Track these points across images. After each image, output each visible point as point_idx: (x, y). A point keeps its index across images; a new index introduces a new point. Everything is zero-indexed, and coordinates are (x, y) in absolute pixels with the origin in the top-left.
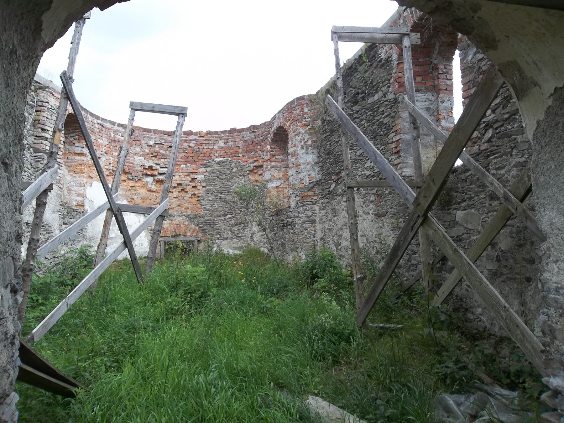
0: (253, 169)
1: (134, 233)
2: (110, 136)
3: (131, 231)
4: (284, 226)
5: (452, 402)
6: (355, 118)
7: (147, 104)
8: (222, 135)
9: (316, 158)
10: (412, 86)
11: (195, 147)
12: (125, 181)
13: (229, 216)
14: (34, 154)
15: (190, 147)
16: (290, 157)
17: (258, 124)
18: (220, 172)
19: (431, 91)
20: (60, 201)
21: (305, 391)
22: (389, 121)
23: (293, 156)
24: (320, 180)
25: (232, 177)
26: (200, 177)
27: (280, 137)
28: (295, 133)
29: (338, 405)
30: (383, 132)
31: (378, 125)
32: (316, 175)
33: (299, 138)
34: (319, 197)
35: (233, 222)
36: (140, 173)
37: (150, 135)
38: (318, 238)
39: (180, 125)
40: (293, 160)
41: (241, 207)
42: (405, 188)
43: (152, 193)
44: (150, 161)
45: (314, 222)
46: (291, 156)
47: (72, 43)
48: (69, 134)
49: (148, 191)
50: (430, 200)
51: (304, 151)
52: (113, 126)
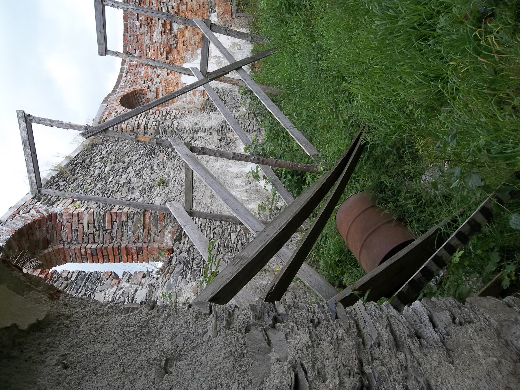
1: (228, 60)
2: (137, 65)
3: (226, 63)
7: (98, 39)
12: (178, 51)
14: (161, 134)
20: (200, 113)
36: (169, 36)
37: (130, 26)
44: (157, 25)
48: (139, 103)
52: (126, 62)
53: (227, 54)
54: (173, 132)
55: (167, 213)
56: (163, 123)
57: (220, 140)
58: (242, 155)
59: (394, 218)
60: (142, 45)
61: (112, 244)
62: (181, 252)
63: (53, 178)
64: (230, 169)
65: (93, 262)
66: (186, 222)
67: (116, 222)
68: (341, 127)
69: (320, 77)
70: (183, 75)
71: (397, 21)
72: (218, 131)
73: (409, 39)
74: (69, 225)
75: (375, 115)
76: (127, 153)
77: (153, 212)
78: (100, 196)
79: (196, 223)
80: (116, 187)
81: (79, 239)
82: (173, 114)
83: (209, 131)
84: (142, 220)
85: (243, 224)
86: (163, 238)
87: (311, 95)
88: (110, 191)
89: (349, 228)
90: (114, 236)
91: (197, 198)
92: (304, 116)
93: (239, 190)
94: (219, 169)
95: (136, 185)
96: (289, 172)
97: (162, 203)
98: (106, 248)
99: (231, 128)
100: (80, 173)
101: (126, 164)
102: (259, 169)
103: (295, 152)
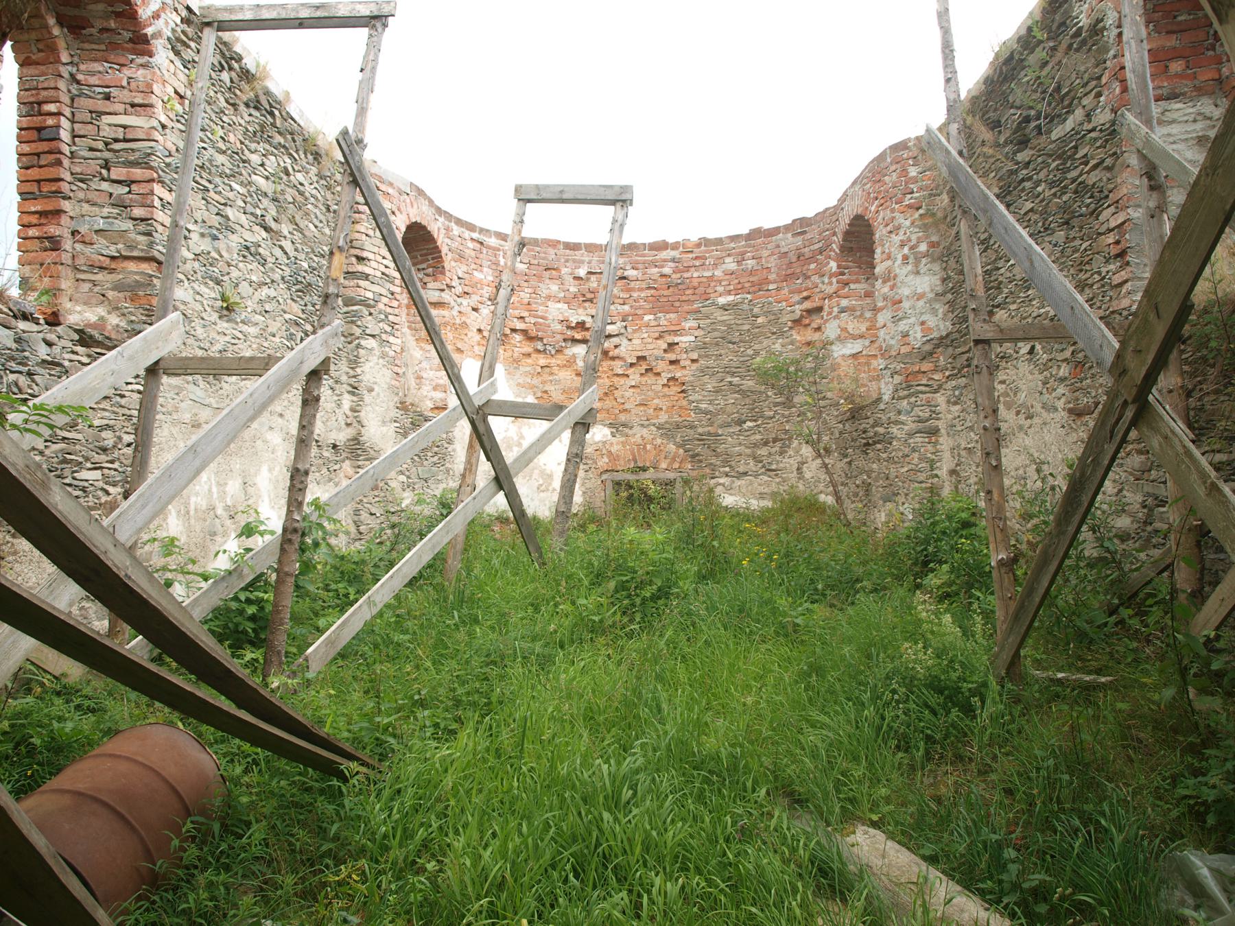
0: (802, 316)
1: (516, 460)
2: (497, 264)
3: (509, 456)
4: (867, 444)
5: (1205, 872)
6: (1023, 180)
7: (547, 186)
8: (732, 245)
9: (938, 282)
10: (1146, 86)
11: (674, 276)
12: (529, 355)
13: (749, 424)
14: (345, 309)
15: (663, 276)
16: (878, 284)
17: (810, 214)
18: (729, 326)
19: (1211, 94)
20: (396, 399)
21: (849, 817)
22: (1101, 180)
23: (884, 282)
24: (947, 335)
25: (756, 336)
26: (685, 340)
27: (858, 240)
28: (888, 228)
29: (922, 852)
30: (1087, 206)
31: (1076, 192)
32: (939, 324)
33: (896, 239)
34: (947, 373)
35: (758, 437)
36: (559, 337)
37: (578, 255)
38: (943, 472)
39: (618, 226)
40: (886, 290)
41: (776, 404)
42: (1096, 333)
44: (580, 311)
45: (934, 432)
46: (880, 281)
47: (362, 70)
50: (1150, 358)
51: (910, 267)
53: (527, 457)
54: (349, 337)
55: (151, 316)
56: (371, 314)
57: (335, 446)
58: (302, 490)
59: (159, 864)
60: (540, 278)
61: (68, 177)
62: (50, 344)
63: (239, 59)
64: (265, 468)
65: (21, 129)
66: (131, 358)
67: (129, 192)
68: (378, 719)
69: (487, 665)
70: (480, 363)
71: (610, 811)
72: (356, 440)
73: (575, 840)
74: (121, 80)
75: (410, 790)
76: (301, 231)
77: (155, 281)
78: (196, 161)
79: (127, 384)
80: (217, 197)
81: (83, 102)
82: (391, 339)
83: (355, 419)
84: (135, 254)
85: (126, 498)
86: (85, 304)
87: (447, 648)
88: (207, 184)
89: (127, 759)
90: (90, 183)
91: (191, 387)
92: (398, 637)
93: (215, 490)
94: (265, 441)
95: (221, 245)
96: (262, 609)
97: (177, 303)
98: (59, 163)
99: (362, 471)
100: (251, 119)
101: (273, 225)
102: (268, 538)
103: (311, 624)
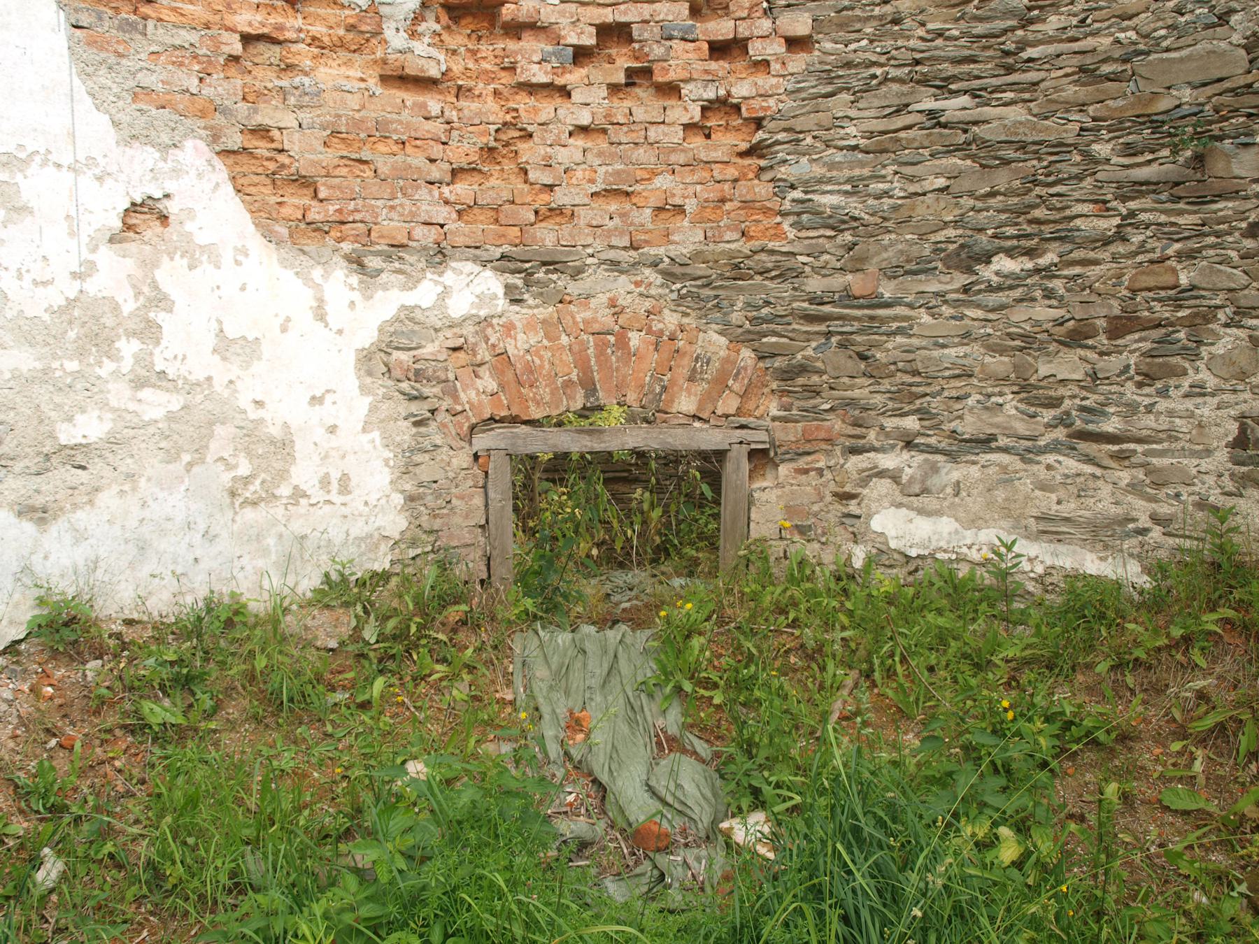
35: (1044, 312)
43: (411, 97)
49: (384, 79)
